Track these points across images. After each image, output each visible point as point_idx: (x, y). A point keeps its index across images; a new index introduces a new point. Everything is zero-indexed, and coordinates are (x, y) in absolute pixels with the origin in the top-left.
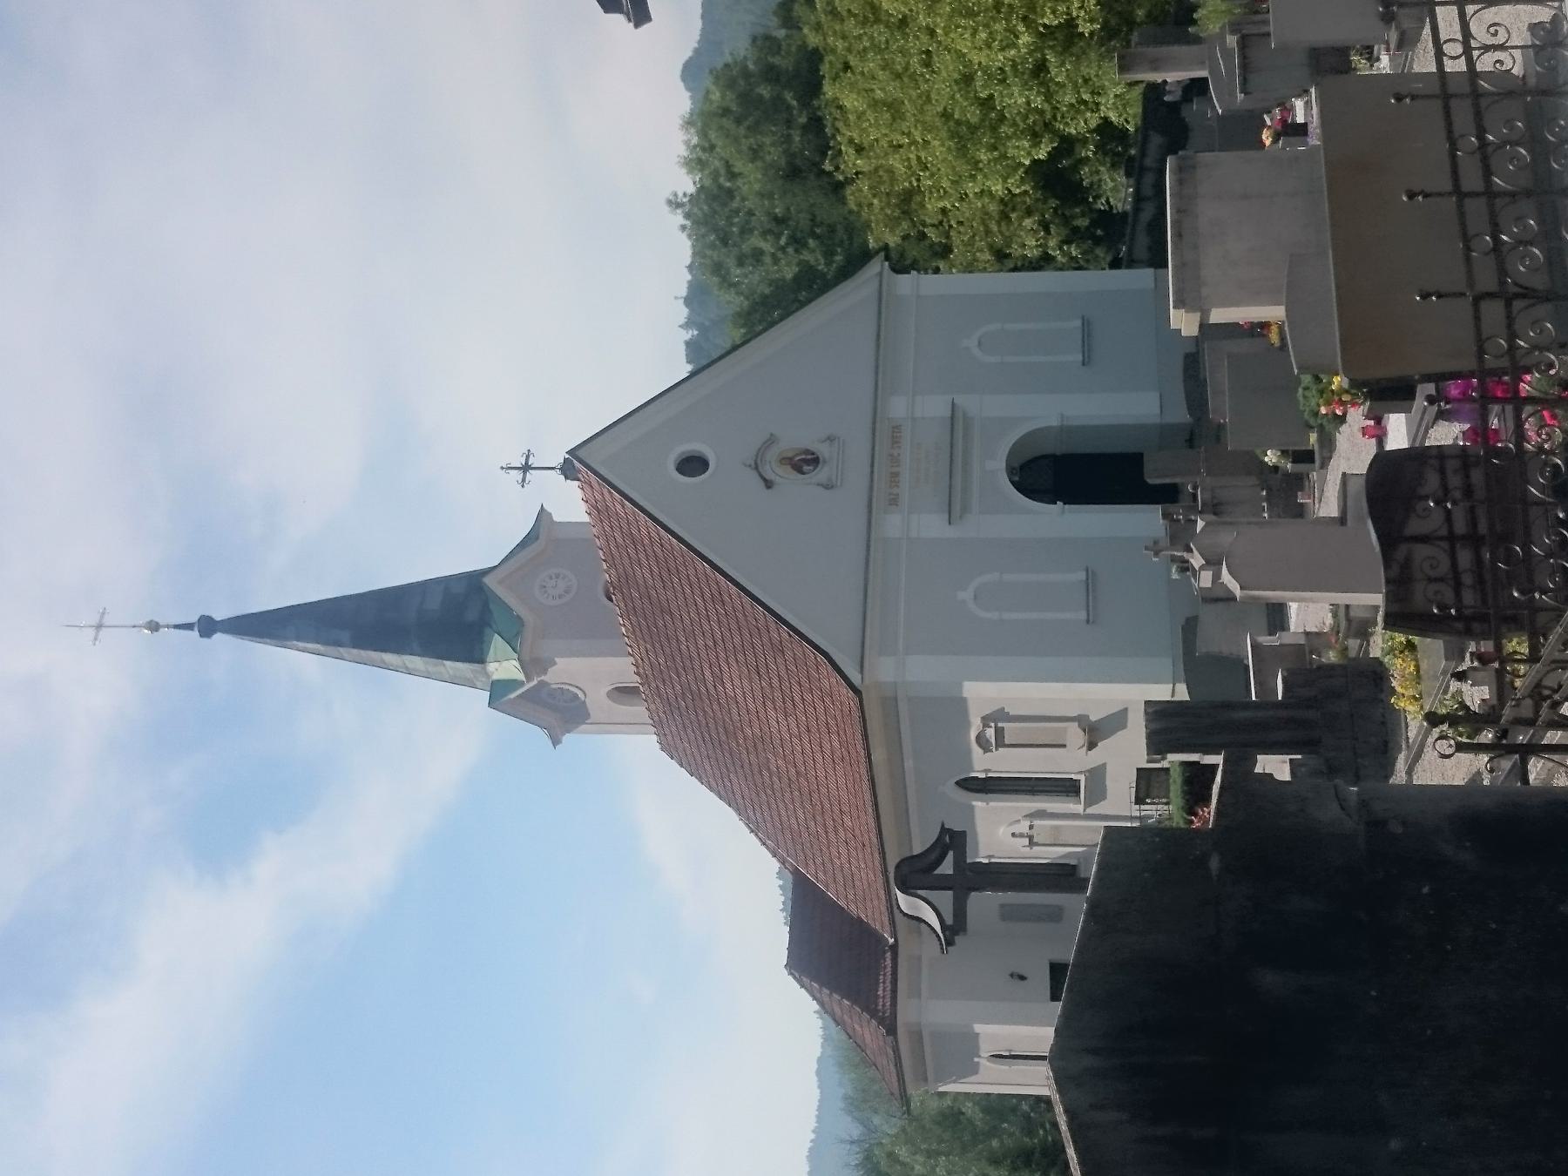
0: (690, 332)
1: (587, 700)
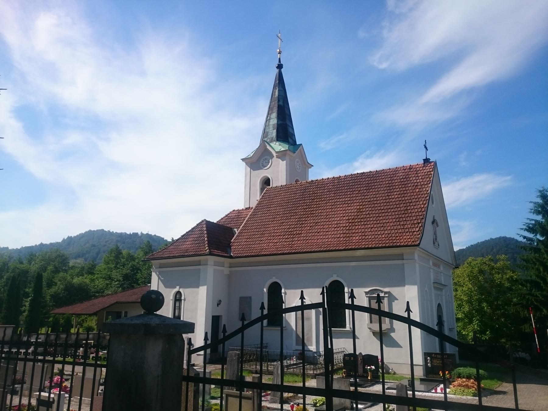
1: (263, 170)
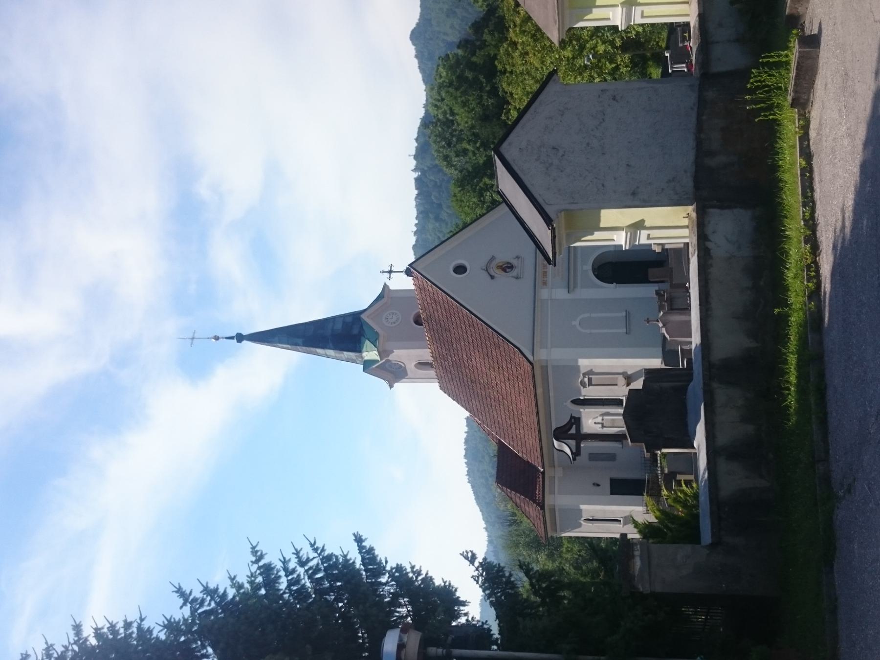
0: (417, 173)
